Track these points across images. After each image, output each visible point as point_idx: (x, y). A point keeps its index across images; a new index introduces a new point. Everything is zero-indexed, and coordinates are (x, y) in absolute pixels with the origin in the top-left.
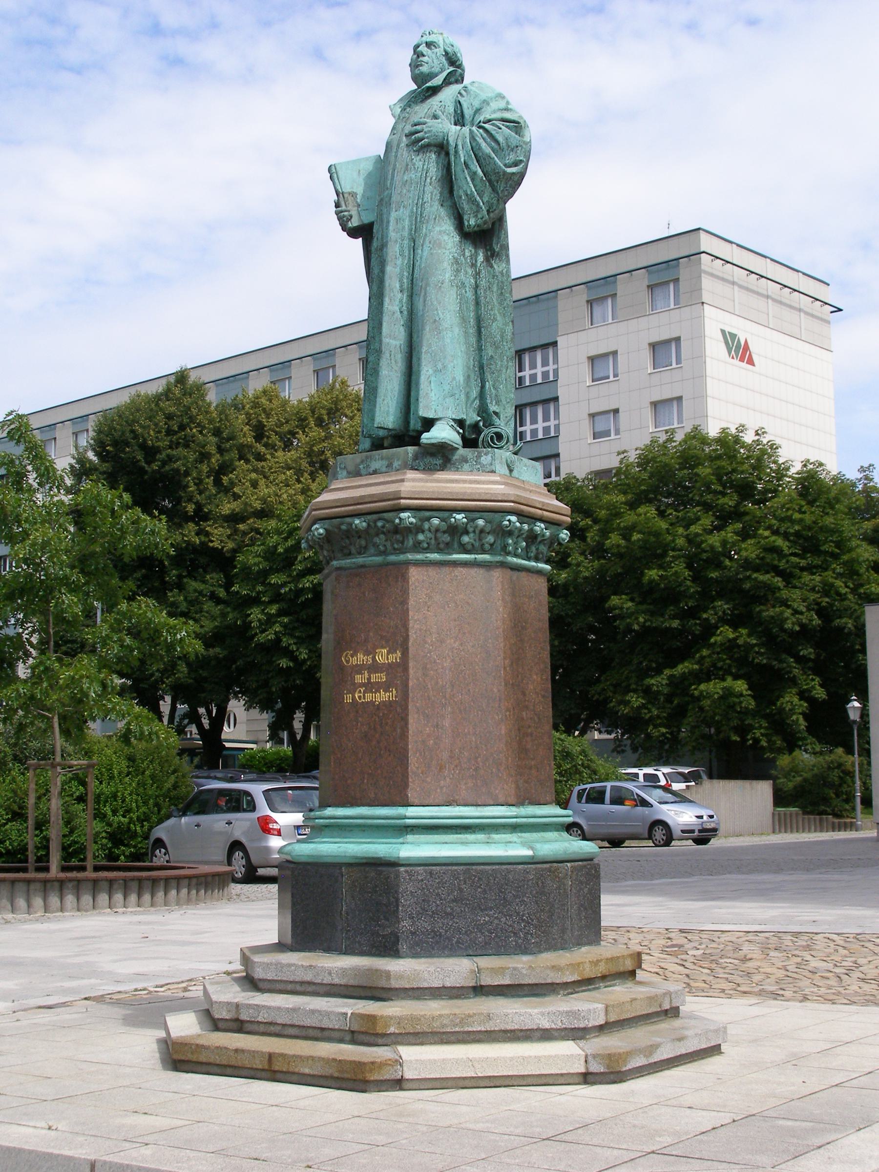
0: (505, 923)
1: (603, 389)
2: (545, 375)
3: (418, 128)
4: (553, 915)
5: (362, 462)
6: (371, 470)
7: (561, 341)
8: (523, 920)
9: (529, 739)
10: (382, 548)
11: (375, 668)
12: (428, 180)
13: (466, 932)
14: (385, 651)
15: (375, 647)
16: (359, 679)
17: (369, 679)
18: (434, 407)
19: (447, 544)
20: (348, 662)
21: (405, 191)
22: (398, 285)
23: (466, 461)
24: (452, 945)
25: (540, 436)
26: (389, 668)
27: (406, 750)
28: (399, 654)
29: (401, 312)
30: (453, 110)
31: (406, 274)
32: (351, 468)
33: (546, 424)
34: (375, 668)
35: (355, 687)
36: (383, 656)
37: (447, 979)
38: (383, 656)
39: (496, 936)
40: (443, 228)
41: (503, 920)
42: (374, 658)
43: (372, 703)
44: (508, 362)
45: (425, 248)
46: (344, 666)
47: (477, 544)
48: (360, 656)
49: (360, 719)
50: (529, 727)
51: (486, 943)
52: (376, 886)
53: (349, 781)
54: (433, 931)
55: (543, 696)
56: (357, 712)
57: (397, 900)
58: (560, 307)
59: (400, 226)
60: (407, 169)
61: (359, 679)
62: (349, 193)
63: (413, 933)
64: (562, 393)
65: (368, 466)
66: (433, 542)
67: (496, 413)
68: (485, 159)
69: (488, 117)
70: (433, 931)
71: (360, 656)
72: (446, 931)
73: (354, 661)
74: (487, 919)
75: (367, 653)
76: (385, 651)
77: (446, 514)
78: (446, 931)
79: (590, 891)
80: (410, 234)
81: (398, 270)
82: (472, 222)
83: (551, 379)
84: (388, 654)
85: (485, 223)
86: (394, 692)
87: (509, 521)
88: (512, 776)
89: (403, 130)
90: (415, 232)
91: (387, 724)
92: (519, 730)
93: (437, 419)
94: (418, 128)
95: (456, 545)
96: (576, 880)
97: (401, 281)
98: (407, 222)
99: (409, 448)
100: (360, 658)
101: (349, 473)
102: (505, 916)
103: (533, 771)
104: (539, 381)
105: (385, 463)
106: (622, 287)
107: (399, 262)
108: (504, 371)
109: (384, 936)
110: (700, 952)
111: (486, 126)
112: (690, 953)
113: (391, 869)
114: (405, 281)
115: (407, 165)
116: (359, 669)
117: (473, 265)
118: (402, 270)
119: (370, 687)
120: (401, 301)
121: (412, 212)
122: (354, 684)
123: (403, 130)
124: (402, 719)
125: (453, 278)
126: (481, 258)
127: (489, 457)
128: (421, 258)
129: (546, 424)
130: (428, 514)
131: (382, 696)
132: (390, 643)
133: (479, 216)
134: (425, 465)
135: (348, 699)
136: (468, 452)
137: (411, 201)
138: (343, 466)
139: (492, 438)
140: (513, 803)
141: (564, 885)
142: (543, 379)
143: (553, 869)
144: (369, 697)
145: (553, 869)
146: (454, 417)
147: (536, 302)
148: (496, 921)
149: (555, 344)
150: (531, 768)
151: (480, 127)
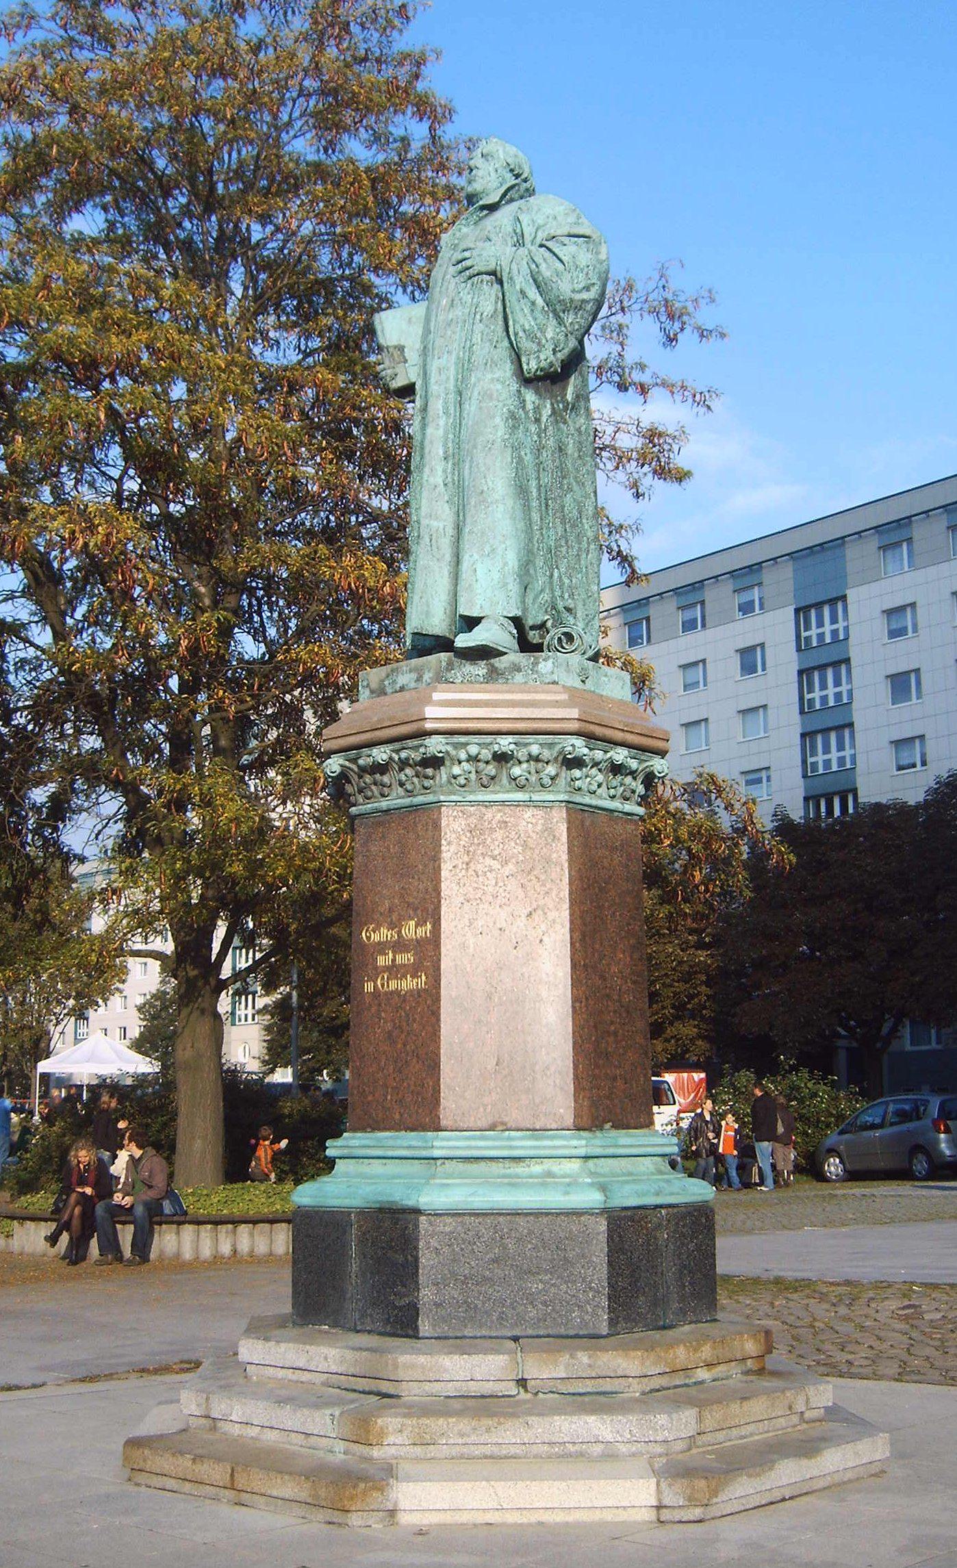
0: (566, 1292)
1: (901, 644)
2: (835, 633)
3: (467, 254)
4: (637, 1280)
5: (388, 676)
6: (398, 687)
7: (851, 595)
8: (591, 1288)
9: (611, 1039)
10: (409, 787)
11: (400, 945)
12: (478, 317)
13: (512, 1304)
14: (412, 923)
15: (401, 919)
16: (381, 961)
17: (394, 960)
18: (479, 602)
19: (493, 778)
20: (369, 938)
21: (449, 333)
22: (441, 452)
23: (519, 670)
24: (492, 1322)
25: (831, 704)
26: (420, 943)
27: (438, 1055)
28: (429, 926)
29: (446, 485)
30: (511, 230)
31: (451, 436)
32: (374, 685)
33: (838, 689)
34: (400, 945)
35: (377, 971)
36: (411, 930)
37: (478, 1369)
38: (411, 930)
39: (553, 1310)
40: (496, 376)
41: (564, 1287)
42: (399, 933)
43: (397, 992)
44: (589, 543)
45: (473, 401)
46: (365, 945)
47: (533, 779)
48: (384, 930)
49: (383, 1015)
50: (612, 1023)
51: (539, 1320)
52: (392, 1240)
53: (370, 1098)
54: (466, 1302)
55: (634, 982)
56: (380, 1005)
57: (416, 1259)
58: (848, 558)
59: (443, 377)
60: (452, 305)
61: (381, 961)
62: (395, 347)
63: (438, 1305)
64: (854, 654)
65: (394, 682)
66: (473, 776)
67: (568, 610)
68: (546, 284)
69: (553, 233)
70: (466, 1302)
71: (384, 930)
72: (484, 1304)
73: (375, 937)
74: (541, 1286)
75: (391, 927)
76: (412, 923)
77: (489, 739)
78: (484, 1304)
79: (698, 1248)
80: (456, 386)
81: (441, 432)
82: (533, 365)
83: (841, 637)
84: (416, 927)
85: (551, 364)
86: (424, 978)
87: (573, 745)
88: (584, 1089)
89: (450, 259)
90: (462, 383)
91: (414, 1020)
92: (595, 1027)
93: (482, 618)
94: (467, 254)
95: (505, 781)
96: (675, 1231)
97: (445, 445)
98: (452, 372)
99: (442, 654)
100: (384, 934)
101: (372, 692)
102: (566, 1282)
103: (619, 1083)
104: (828, 640)
105: (414, 676)
106: (919, 532)
107: (442, 422)
108: (584, 556)
109: (401, 1308)
110: (939, 1316)
111: (549, 244)
112: (927, 1317)
113: (413, 1216)
114: (450, 445)
115: (453, 301)
116: (382, 948)
117: (537, 421)
118: (446, 433)
119: (395, 971)
120: (445, 471)
121: (458, 358)
122: (376, 968)
123: (450, 259)
124: (433, 1013)
125: (507, 437)
126: (546, 412)
127: (550, 663)
128: (468, 414)
129: (838, 689)
130: (463, 739)
131: (408, 984)
132: (419, 912)
133: (542, 357)
134: (464, 676)
135: (369, 987)
136: (523, 659)
137: (456, 345)
138: (365, 683)
139: (560, 639)
140: (586, 1126)
141: (655, 1238)
142: (832, 638)
143: (636, 1218)
144: (393, 985)
145: (636, 1218)
146: (505, 614)
147: (818, 552)
148: (553, 1290)
149: (843, 598)
150: (615, 1079)
151: (541, 246)
